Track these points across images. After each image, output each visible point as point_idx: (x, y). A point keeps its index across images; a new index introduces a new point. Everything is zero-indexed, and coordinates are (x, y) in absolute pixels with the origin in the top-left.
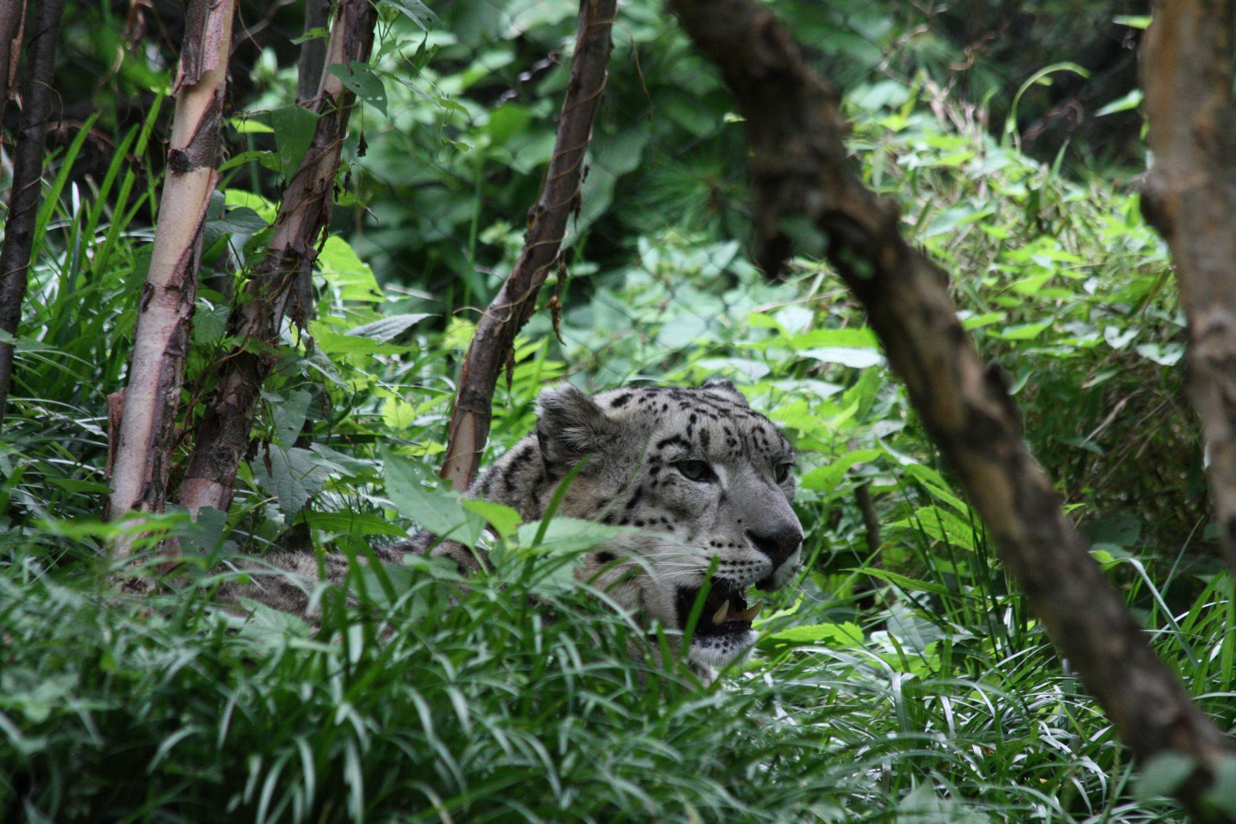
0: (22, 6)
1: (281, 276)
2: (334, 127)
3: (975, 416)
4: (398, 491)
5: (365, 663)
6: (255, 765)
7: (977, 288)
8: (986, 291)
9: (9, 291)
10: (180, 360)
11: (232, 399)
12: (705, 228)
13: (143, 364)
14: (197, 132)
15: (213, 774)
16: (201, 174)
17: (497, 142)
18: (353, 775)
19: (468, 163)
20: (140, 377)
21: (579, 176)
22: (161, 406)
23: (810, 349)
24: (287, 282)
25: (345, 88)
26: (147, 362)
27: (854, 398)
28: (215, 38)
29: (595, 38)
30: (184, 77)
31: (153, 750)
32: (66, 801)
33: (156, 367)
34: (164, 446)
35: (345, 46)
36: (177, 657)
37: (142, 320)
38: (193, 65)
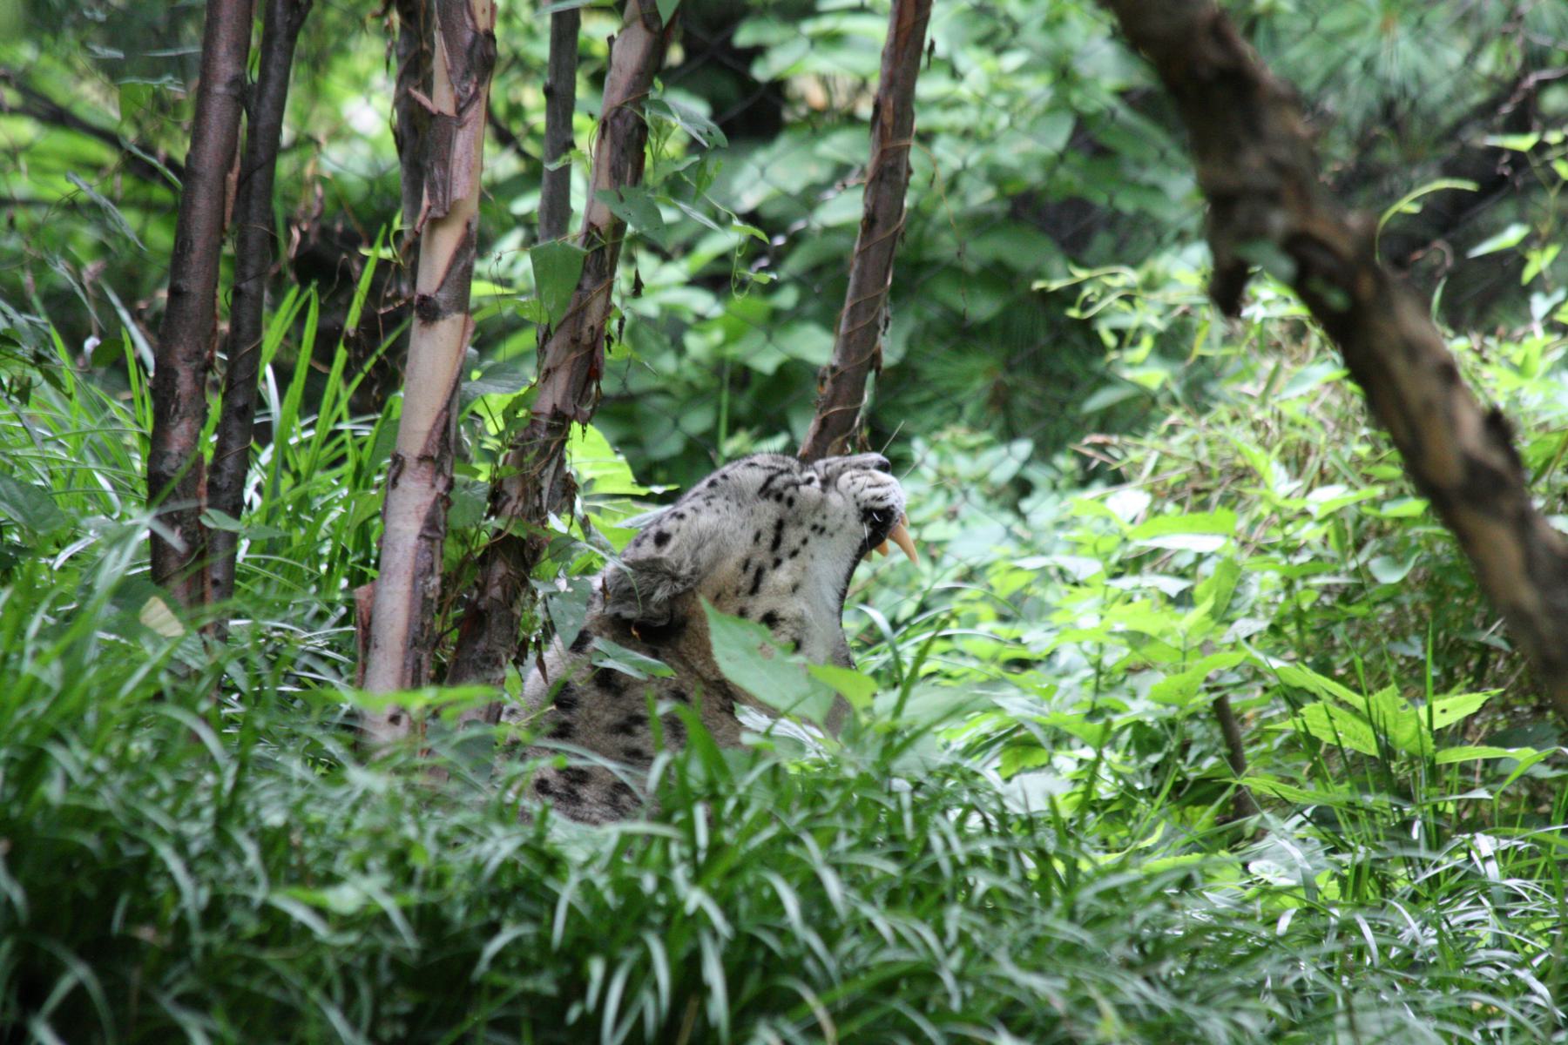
1: (548, 443)
3: (1474, 468)
4: (728, 659)
5: (716, 848)
6: (596, 968)
7: (1347, 458)
8: (1358, 462)
11: (496, 592)
12: (988, 427)
13: (395, 550)
15: (546, 985)
17: (732, 337)
18: (714, 974)
19: (697, 363)
20: (392, 566)
21: (878, 328)
22: (419, 599)
23: (1153, 538)
24: (555, 451)
25: (612, 214)
26: (399, 547)
27: (1209, 592)
28: (465, 161)
29: (890, 163)
30: (429, 208)
31: (475, 957)
32: (376, 1019)
33: (410, 553)
34: (424, 646)
36: (497, 848)
37: (391, 498)
38: (440, 194)
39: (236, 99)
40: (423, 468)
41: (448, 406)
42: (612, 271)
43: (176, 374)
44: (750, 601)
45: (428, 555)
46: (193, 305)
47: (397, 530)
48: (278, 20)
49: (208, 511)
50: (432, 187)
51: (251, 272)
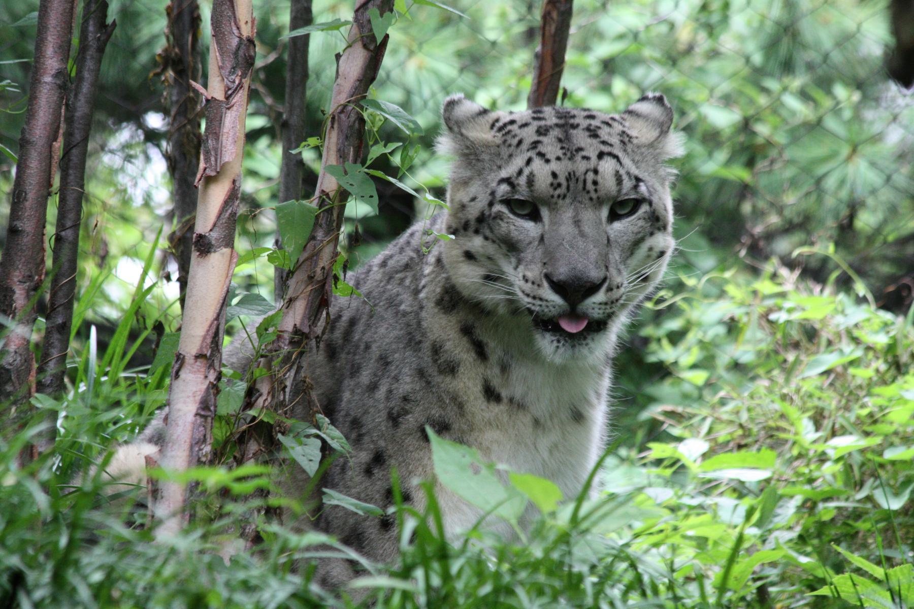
1: (289, 355)
2: (331, 221)
10: (209, 419)
13: (177, 425)
14: (219, 217)
16: (223, 254)
20: (174, 437)
23: (715, 471)
24: (296, 359)
26: (180, 422)
28: (231, 134)
30: (205, 169)
33: (189, 428)
35: (339, 150)
36: (273, 596)
38: (213, 159)
40: (198, 363)
43: (13, 292)
44: (559, 180)
45: (202, 429)
46: (26, 241)
47: (179, 410)
48: (91, 37)
49: (37, 395)
50: (207, 153)
51: (69, 223)
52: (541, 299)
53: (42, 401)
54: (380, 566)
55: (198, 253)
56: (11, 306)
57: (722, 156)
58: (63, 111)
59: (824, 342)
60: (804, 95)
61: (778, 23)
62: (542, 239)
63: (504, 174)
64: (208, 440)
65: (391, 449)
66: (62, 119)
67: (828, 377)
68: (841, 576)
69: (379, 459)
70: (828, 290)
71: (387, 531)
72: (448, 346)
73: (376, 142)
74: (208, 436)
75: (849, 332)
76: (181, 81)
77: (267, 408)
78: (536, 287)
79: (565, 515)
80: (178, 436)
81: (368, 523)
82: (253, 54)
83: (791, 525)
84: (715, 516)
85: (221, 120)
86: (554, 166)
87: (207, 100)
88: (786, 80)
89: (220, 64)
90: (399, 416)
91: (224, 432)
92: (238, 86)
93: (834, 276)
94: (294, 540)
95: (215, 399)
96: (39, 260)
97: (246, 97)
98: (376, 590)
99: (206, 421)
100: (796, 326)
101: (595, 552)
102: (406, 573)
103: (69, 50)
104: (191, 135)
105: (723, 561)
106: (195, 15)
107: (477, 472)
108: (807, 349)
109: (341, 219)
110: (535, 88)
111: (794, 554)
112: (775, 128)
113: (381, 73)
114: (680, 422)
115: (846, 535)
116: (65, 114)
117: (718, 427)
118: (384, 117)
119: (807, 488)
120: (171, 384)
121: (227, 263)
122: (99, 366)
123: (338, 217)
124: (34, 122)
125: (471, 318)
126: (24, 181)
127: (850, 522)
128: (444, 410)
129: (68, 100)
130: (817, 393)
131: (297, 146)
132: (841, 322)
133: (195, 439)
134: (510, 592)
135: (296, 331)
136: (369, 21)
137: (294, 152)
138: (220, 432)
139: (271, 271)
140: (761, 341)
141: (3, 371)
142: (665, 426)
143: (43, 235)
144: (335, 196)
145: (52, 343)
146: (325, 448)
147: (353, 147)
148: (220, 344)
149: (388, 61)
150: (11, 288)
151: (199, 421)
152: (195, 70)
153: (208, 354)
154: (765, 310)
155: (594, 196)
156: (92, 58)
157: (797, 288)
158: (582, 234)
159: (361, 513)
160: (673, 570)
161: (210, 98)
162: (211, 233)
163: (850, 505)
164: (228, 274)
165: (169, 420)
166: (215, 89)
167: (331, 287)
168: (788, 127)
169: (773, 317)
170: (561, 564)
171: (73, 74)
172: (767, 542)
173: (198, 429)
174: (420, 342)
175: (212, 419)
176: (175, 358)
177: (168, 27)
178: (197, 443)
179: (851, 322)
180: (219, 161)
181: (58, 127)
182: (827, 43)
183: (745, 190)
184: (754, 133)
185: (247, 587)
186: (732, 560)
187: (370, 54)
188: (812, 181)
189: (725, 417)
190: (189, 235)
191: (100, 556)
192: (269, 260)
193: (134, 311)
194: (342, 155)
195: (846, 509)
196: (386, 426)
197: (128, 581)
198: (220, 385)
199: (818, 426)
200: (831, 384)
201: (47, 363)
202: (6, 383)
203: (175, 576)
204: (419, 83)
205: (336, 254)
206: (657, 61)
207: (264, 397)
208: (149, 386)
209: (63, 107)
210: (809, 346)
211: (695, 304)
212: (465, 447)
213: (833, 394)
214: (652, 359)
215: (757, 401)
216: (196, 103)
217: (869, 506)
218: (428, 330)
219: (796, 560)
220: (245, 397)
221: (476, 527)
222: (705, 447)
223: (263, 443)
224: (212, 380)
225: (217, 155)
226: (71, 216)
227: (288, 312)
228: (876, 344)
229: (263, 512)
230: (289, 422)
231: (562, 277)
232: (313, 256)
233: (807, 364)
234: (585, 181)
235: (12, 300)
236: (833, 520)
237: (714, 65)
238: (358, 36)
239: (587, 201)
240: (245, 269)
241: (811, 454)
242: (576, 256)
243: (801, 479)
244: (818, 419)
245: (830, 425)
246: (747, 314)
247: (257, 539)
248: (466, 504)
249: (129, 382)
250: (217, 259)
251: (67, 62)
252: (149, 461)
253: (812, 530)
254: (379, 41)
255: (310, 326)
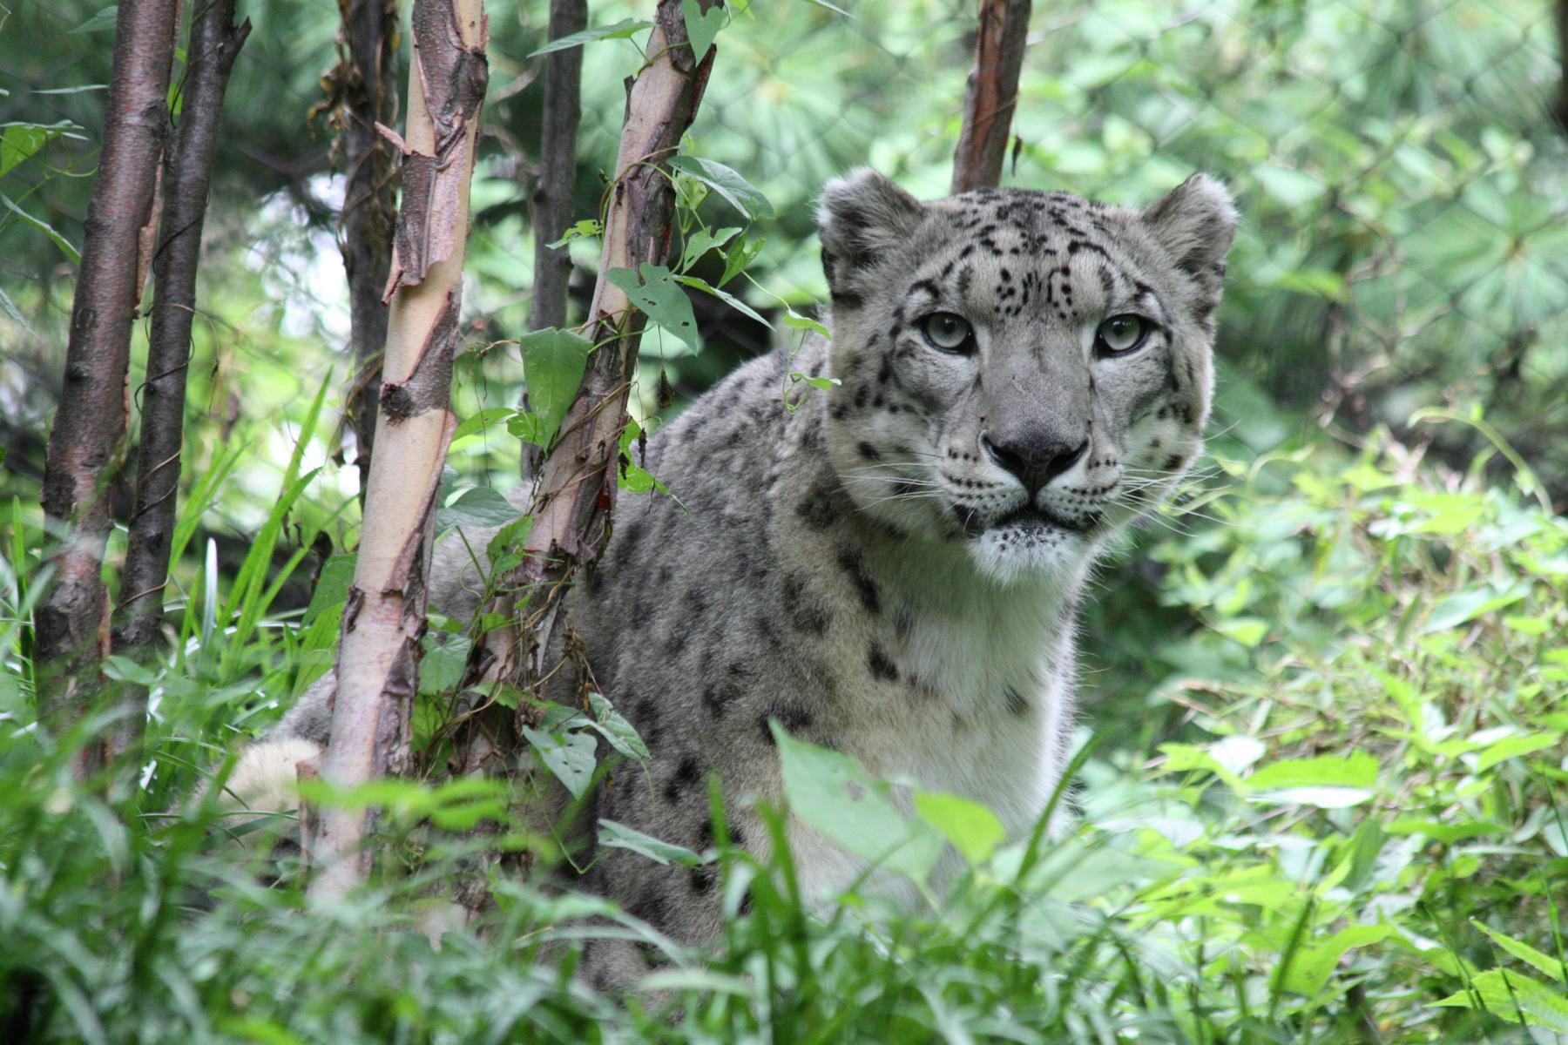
0: (155, 177)
1: (545, 590)
9: (137, 624)
10: (406, 701)
13: (351, 710)
20: (346, 731)
24: (554, 599)
25: (631, 305)
26: (356, 706)
28: (446, 214)
30: (401, 274)
33: (371, 715)
35: (630, 243)
36: (507, 1004)
38: (414, 256)
39: (154, 133)
40: (388, 605)
41: (421, 528)
42: (629, 374)
43: (73, 482)
44: (1011, 284)
45: (393, 717)
46: (95, 394)
47: (354, 685)
48: (207, 47)
49: (111, 658)
51: (168, 366)
52: (980, 485)
53: (119, 669)
54: (692, 952)
55: (388, 418)
56: (69, 505)
57: (1291, 253)
58: (159, 174)
59: (1462, 572)
60: (1434, 148)
61: (1388, 26)
62: (978, 381)
63: (923, 274)
64: (404, 736)
65: (710, 754)
66: (158, 188)
67: (1469, 633)
68: (1486, 973)
69: (688, 772)
70: (1473, 481)
71: (702, 895)
72: (815, 584)
73: (695, 228)
74: (404, 730)
75: (1506, 556)
76: (362, 122)
77: (505, 682)
78: (970, 462)
79: (1008, 863)
80: (353, 729)
81: (671, 882)
82: (483, 77)
83: (1408, 885)
84: (1275, 868)
85: (428, 191)
86: (1006, 261)
87: (406, 158)
88: (1402, 124)
89: (427, 95)
90: (723, 699)
91: (432, 721)
92: (457, 132)
93: (1482, 459)
94: (543, 906)
95: (417, 667)
96: (116, 428)
97: (471, 151)
98: (684, 993)
99: (400, 705)
100: (1415, 546)
101: (1060, 931)
102: (735, 965)
103: (169, 71)
104: (381, 216)
105: (1282, 944)
106: (388, 10)
107: (856, 794)
108: (1434, 584)
109: (633, 355)
110: (967, 136)
111: (1409, 935)
112: (1385, 206)
113: (703, 111)
114: (1217, 708)
115: (1497, 903)
116: (163, 180)
117: (1281, 717)
118: (707, 186)
119: (1432, 821)
120: (341, 641)
121: (439, 433)
122: (222, 608)
123: (628, 357)
124: (110, 193)
125: (857, 542)
126: (92, 293)
127: (1507, 880)
128: (801, 692)
129: (167, 155)
130: (1451, 660)
131: (560, 237)
132: (1493, 539)
133: (381, 734)
134: (912, 995)
135: (556, 551)
136: (683, 22)
137: (553, 246)
138: (425, 724)
139: (516, 447)
140: (1358, 570)
141: (55, 617)
142: (1190, 715)
143: (125, 385)
144: (623, 321)
145: (140, 570)
146: (604, 749)
147: (655, 236)
148: (424, 572)
149: (718, 86)
150: (69, 476)
151: (388, 704)
152: (387, 104)
153: (405, 590)
154: (1363, 516)
155: (1067, 310)
156: (210, 84)
157: (1419, 481)
158: (1044, 369)
159: (664, 861)
160: (1201, 962)
161: (409, 153)
162: (411, 383)
163: (1506, 850)
164: (438, 453)
165: (338, 702)
166: (417, 136)
167: (615, 475)
168: (1406, 205)
169: (1376, 528)
170: (1001, 950)
171: (177, 111)
172: (1365, 913)
173: (385, 719)
174: (764, 573)
175: (411, 700)
176: (349, 597)
177: (341, 30)
178: (385, 741)
179: (1509, 538)
180: (424, 260)
181: (151, 202)
182: (1474, 59)
183: (1333, 312)
184: (1347, 216)
185: (463, 987)
186: (1295, 943)
187: (684, 77)
188: (1445, 296)
189: (1294, 700)
190: (374, 386)
191: (212, 933)
192: (510, 430)
193: (281, 516)
194: (635, 251)
195: (1499, 857)
196: (701, 716)
197: (261, 977)
198: (424, 642)
199: (1450, 715)
200: (1476, 645)
201: (129, 604)
202: (59, 638)
203: (340, 969)
204: (777, 126)
205: (625, 420)
206: (1181, 91)
207: (500, 664)
208: (305, 644)
209: (160, 168)
210: (1437, 579)
211: (1243, 506)
212: (837, 755)
213: (1480, 663)
214: (1171, 600)
215: (1347, 674)
216: (388, 161)
217: (1539, 852)
218: (780, 554)
219: (1411, 945)
220: (468, 664)
221: (853, 890)
222: (1258, 750)
223: (499, 743)
224: (411, 634)
225: (421, 250)
226: (173, 353)
227: (541, 518)
228: (1550, 576)
229: (497, 861)
230: (543, 707)
231: (1011, 437)
232: (586, 423)
233: (1433, 610)
234: (1050, 288)
235: (71, 496)
236: (1477, 877)
237: (1281, 98)
238: (664, 47)
239: (1056, 320)
240: (471, 445)
241: (1439, 763)
242: (1036, 403)
243: (1421, 807)
244: (1451, 705)
245: (1472, 714)
246: (1334, 524)
247: (483, 905)
248: (840, 850)
249: (273, 637)
250: (422, 427)
251: (167, 91)
252: (303, 770)
253: (1440, 895)
254: (699, 59)
255: (579, 542)
